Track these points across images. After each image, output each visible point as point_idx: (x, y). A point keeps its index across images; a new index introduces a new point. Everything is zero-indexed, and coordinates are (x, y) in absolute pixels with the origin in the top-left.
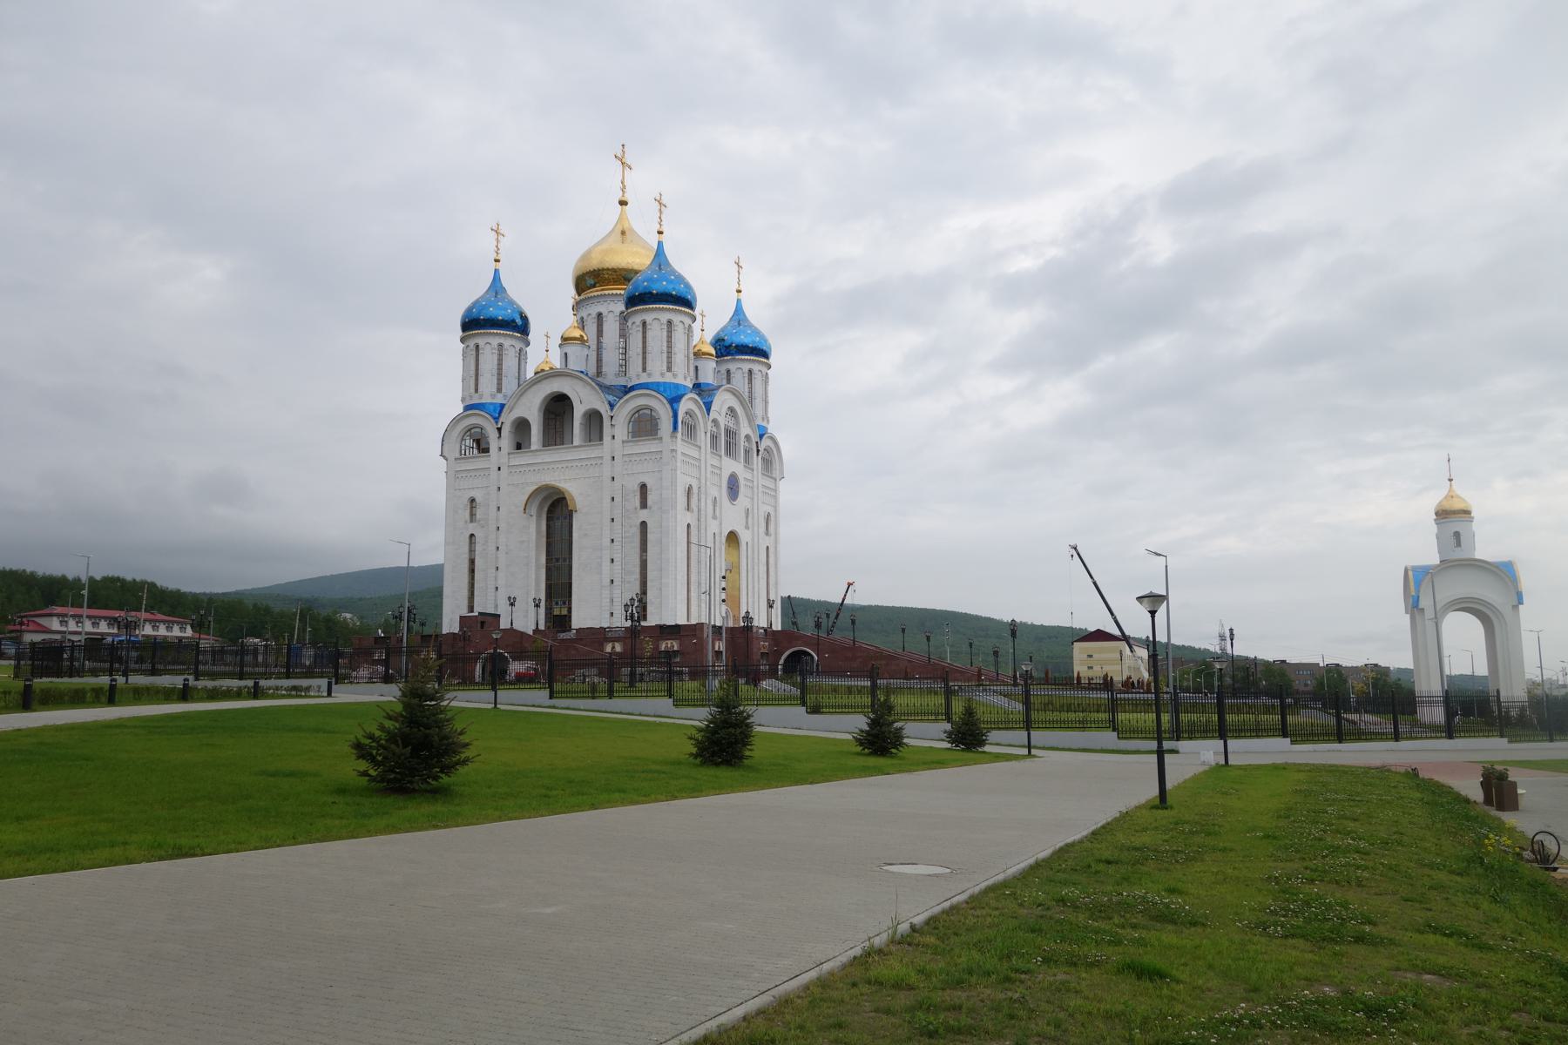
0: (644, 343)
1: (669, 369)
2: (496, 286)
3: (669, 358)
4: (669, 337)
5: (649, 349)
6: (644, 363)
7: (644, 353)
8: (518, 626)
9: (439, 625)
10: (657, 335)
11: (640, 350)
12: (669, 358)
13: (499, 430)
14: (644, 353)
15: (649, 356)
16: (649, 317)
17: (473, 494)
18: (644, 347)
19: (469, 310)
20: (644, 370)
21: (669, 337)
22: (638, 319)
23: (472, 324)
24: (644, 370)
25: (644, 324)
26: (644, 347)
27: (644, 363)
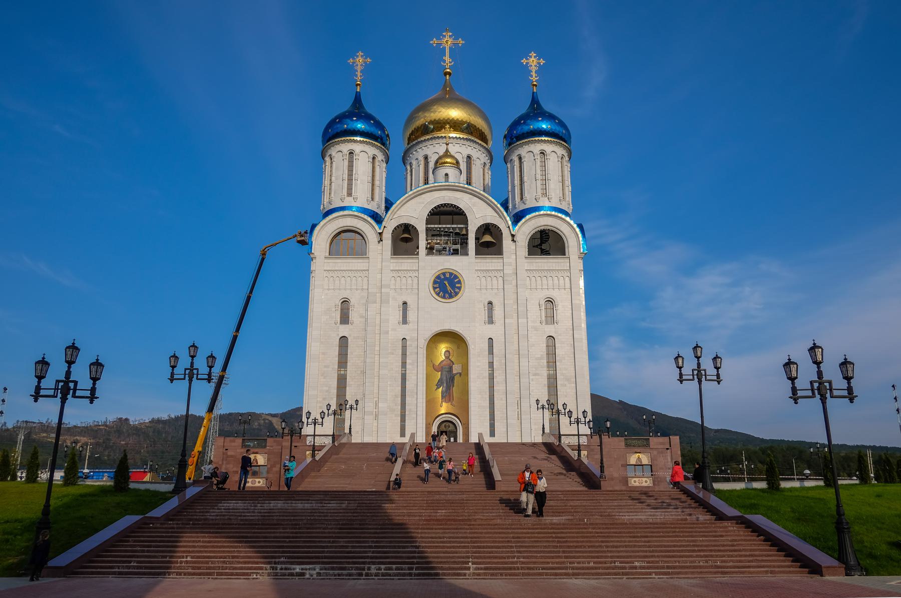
25: (351, 153)
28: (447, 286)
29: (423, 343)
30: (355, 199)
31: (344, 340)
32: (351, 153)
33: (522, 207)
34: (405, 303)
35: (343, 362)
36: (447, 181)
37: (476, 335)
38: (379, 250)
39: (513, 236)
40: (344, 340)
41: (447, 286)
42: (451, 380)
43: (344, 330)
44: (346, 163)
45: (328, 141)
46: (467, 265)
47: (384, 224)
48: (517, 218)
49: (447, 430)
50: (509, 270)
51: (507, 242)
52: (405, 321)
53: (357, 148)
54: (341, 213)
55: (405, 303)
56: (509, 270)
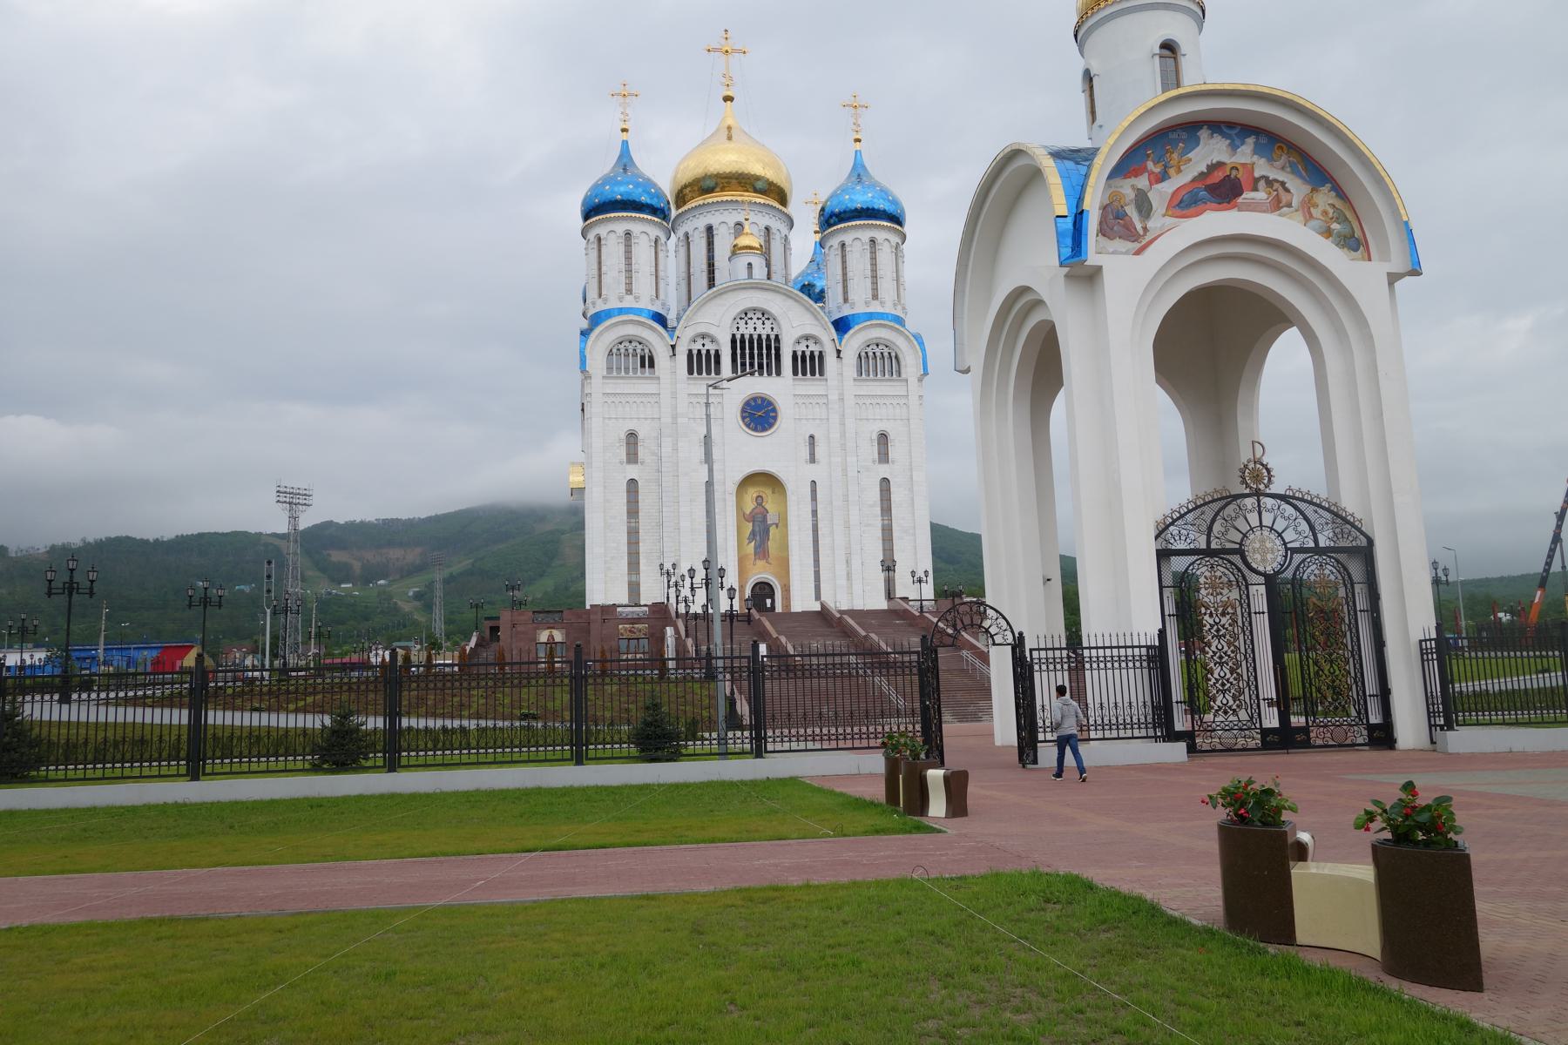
0: (844, 268)
1: (875, 297)
2: (625, 161)
3: (875, 283)
4: (874, 259)
5: (850, 275)
6: (845, 292)
7: (845, 281)
8: (840, 599)
9: (1256, 143)
10: (858, 262)
11: (840, 278)
12: (875, 283)
13: (673, 347)
14: (845, 281)
15: (851, 284)
16: (848, 238)
17: (632, 425)
18: (845, 274)
19: (583, 204)
20: (846, 300)
21: (874, 259)
22: (835, 242)
23: (594, 210)
24: (846, 300)
25: (843, 245)
26: (845, 274)
27: (845, 292)
28: (759, 415)
29: (732, 487)
30: (605, 301)
31: (632, 483)
32: (628, 234)
33: (601, 306)
34: (812, 437)
35: (633, 511)
36: (750, 275)
37: (795, 475)
38: (671, 369)
39: (839, 352)
40: (632, 483)
41: (759, 415)
42: (761, 531)
43: (633, 472)
44: (622, 248)
45: (830, 226)
46: (779, 388)
47: (677, 333)
48: (842, 325)
49: (763, 591)
50: (834, 397)
51: (830, 359)
52: (813, 460)
53: (636, 228)
54: (625, 317)
55: (812, 437)
56: (834, 397)
